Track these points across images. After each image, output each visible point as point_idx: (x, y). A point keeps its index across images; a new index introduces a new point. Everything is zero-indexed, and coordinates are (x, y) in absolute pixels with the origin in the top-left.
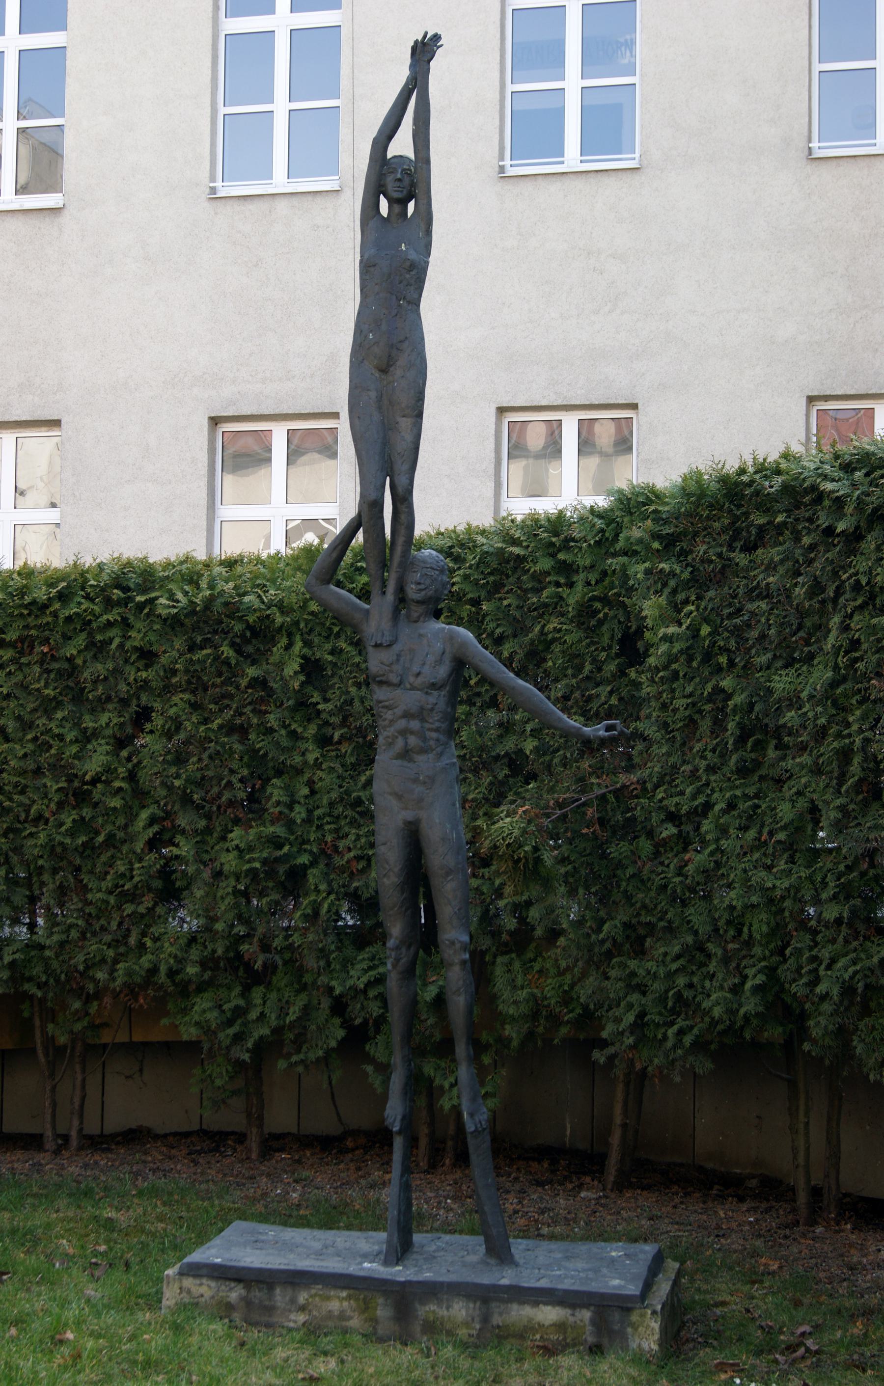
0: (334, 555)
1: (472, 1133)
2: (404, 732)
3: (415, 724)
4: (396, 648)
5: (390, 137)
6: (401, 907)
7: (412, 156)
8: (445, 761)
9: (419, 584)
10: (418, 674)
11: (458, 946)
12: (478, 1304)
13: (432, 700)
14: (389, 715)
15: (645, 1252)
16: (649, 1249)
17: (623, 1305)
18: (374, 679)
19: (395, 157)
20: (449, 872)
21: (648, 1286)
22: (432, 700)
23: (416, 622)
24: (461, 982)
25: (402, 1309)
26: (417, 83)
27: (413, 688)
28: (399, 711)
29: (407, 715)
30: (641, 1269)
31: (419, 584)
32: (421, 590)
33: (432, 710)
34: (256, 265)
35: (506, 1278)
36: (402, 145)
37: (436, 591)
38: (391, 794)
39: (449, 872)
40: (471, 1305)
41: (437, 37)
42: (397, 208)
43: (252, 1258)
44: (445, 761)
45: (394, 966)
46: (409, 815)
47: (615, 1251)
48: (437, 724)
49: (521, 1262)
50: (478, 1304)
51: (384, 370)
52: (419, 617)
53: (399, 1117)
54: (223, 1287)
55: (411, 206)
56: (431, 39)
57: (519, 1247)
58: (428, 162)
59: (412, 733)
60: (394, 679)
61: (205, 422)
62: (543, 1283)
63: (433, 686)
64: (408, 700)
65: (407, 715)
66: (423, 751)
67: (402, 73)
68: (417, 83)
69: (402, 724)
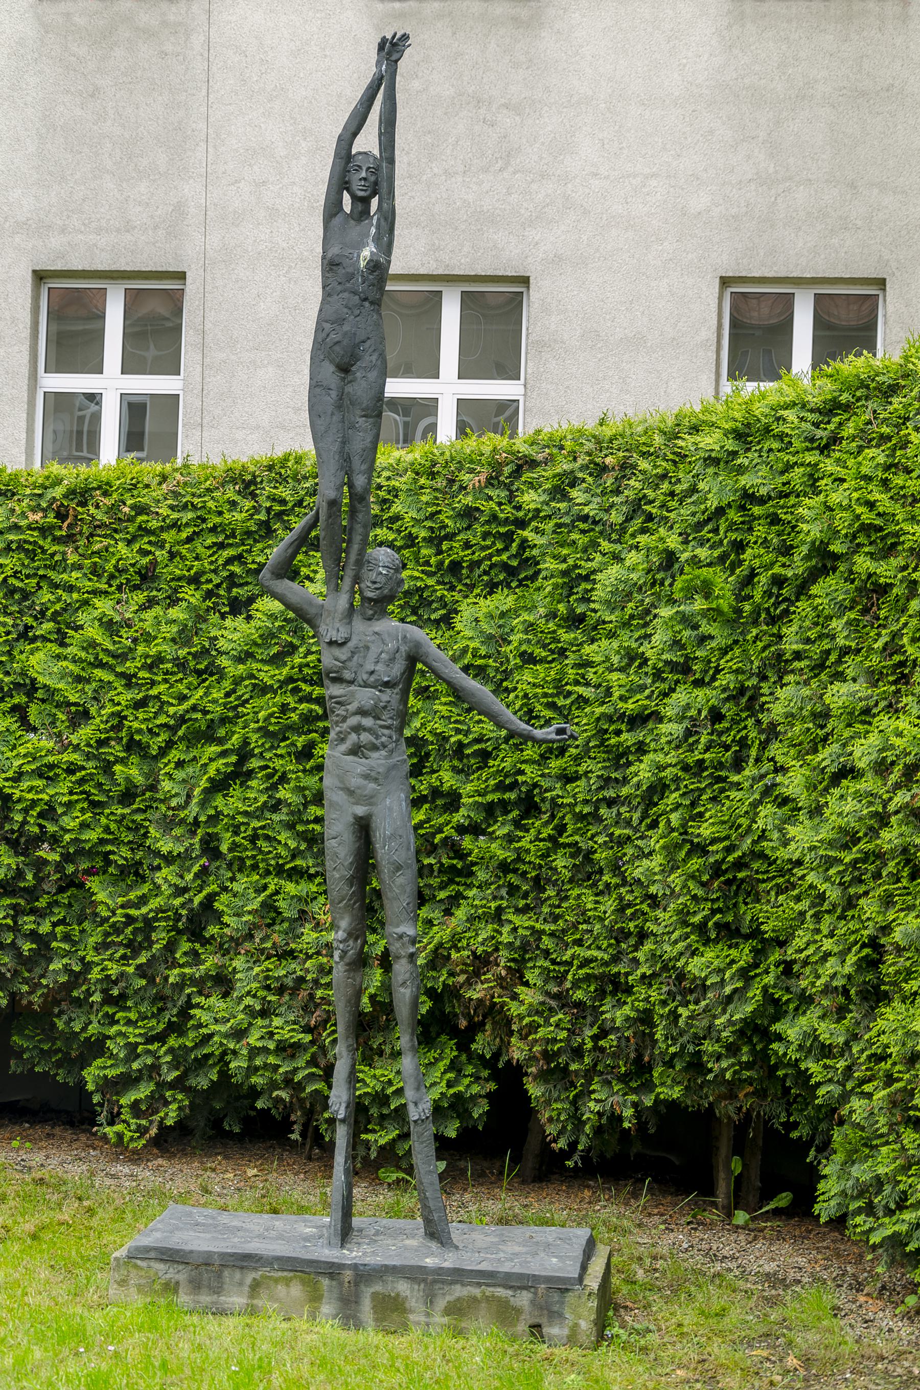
0: (290, 551)
1: (415, 1122)
2: (357, 729)
3: (368, 722)
4: (351, 644)
5: (355, 134)
6: (350, 900)
7: (376, 152)
8: (396, 758)
9: (375, 583)
10: (372, 673)
11: (406, 939)
12: (422, 1286)
13: (385, 697)
14: (341, 711)
15: (577, 1237)
16: (583, 1233)
17: (562, 1286)
18: (327, 675)
19: (360, 153)
20: (399, 868)
21: (584, 1268)
22: (385, 697)
23: (370, 619)
24: (408, 975)
25: (353, 1292)
26: (383, 84)
27: (366, 685)
28: (352, 707)
29: (362, 712)
30: (577, 1252)
31: (375, 583)
32: (377, 589)
33: (385, 708)
34: (92, 96)
35: (449, 1261)
36: (367, 142)
37: (391, 590)
38: (342, 789)
39: (399, 868)
40: (416, 1287)
41: (405, 37)
42: (360, 207)
43: (200, 1242)
44: (396, 758)
45: (341, 958)
46: (360, 810)
47: (550, 1234)
48: (390, 722)
49: (461, 1246)
50: (422, 1286)
51: (345, 369)
52: (373, 615)
53: (344, 1106)
54: (171, 1270)
55: (375, 202)
56: (399, 39)
57: (456, 1231)
58: (391, 161)
59: (365, 730)
60: (347, 675)
61: (29, 277)
62: (484, 1266)
63: (387, 684)
64: (365, 697)
65: (362, 712)
66: (375, 748)
67: (367, 65)
68: (383, 84)
69: (354, 720)
